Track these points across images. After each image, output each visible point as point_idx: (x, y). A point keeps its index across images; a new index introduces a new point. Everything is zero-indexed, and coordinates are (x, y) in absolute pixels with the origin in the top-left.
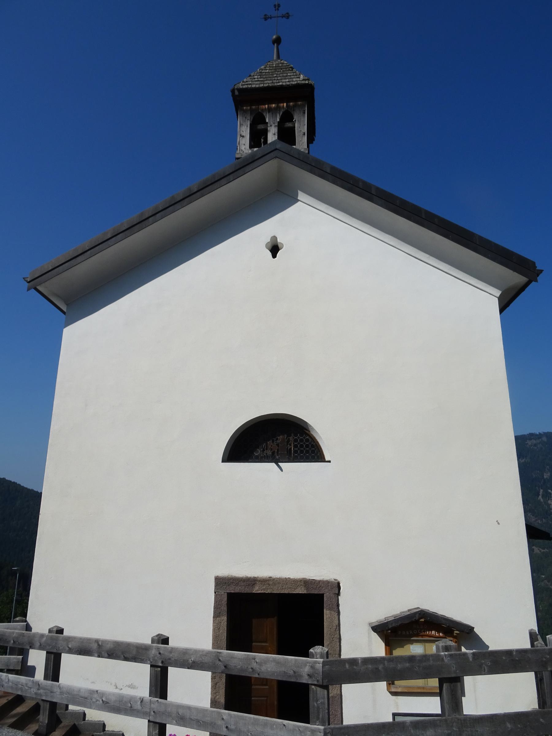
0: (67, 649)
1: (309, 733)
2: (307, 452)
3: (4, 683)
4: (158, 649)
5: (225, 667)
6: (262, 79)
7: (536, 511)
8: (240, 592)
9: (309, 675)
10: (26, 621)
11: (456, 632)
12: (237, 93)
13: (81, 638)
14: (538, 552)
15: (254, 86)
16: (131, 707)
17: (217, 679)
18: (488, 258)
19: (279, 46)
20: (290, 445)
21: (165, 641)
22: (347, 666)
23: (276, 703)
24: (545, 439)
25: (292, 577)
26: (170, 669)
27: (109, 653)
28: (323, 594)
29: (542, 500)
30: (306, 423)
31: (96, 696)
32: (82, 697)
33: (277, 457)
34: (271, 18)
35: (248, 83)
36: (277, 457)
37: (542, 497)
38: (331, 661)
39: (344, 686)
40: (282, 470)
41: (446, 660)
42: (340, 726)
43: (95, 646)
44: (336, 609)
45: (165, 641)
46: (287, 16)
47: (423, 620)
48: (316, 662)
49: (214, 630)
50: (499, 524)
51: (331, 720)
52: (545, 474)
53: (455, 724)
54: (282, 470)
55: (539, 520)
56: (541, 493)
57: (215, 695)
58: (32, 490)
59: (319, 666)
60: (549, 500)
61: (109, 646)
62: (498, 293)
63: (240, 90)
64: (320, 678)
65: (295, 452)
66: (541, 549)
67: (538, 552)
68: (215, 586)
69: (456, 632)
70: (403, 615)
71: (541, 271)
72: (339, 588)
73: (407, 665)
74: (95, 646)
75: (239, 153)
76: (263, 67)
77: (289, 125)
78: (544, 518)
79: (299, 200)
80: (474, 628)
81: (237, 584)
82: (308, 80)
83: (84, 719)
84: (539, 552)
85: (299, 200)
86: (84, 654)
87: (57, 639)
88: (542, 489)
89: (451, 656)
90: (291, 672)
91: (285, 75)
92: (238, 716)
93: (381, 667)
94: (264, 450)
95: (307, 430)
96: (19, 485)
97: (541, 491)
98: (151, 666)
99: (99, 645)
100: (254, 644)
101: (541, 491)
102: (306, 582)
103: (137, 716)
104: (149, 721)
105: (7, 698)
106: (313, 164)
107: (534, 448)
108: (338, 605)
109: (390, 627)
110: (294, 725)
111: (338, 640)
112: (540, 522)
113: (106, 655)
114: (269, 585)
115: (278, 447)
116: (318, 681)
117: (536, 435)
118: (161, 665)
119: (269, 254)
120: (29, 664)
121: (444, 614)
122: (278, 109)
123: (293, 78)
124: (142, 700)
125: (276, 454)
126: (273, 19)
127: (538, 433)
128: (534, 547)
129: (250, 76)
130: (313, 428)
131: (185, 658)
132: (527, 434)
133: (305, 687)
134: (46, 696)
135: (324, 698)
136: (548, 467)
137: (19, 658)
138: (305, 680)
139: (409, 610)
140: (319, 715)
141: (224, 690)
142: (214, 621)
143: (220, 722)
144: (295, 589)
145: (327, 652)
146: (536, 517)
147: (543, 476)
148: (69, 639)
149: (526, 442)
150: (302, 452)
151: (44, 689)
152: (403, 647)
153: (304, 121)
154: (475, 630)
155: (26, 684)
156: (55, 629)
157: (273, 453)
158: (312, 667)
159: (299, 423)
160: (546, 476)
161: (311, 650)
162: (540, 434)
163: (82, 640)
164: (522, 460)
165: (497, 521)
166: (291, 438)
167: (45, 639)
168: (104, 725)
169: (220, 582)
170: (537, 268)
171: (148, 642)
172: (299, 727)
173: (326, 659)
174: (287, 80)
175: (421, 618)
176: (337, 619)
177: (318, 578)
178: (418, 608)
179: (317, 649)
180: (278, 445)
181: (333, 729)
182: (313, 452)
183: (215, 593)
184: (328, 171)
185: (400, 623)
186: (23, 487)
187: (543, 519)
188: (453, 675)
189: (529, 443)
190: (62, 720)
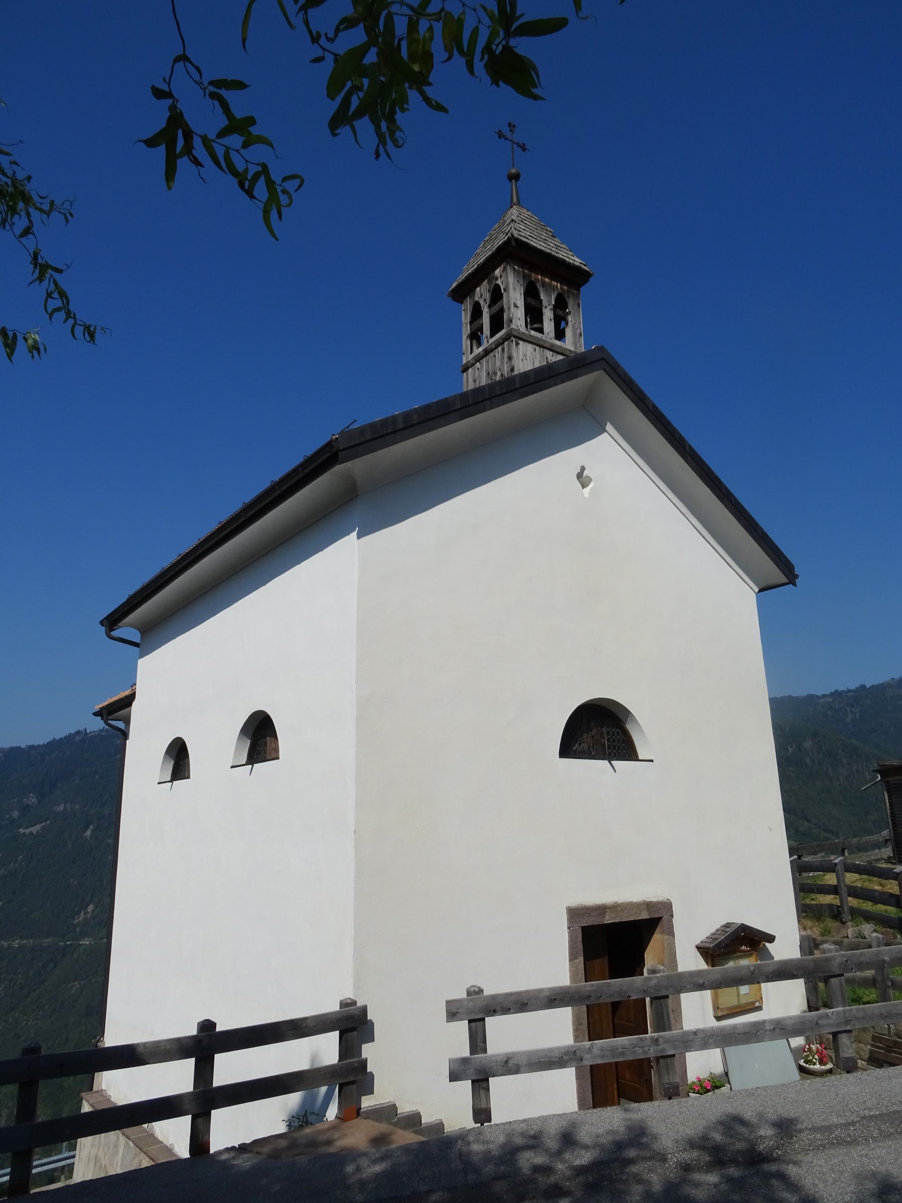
20: (604, 738)
27: (849, 962)
32: (739, 1034)
33: (593, 753)
94: (580, 744)
95: (623, 723)
102: (649, 905)
106: (638, 394)
114: (618, 912)
115: (593, 740)
122: (554, 288)
130: (634, 720)
159: (614, 710)
169: (574, 913)
178: (728, 925)
180: (593, 737)
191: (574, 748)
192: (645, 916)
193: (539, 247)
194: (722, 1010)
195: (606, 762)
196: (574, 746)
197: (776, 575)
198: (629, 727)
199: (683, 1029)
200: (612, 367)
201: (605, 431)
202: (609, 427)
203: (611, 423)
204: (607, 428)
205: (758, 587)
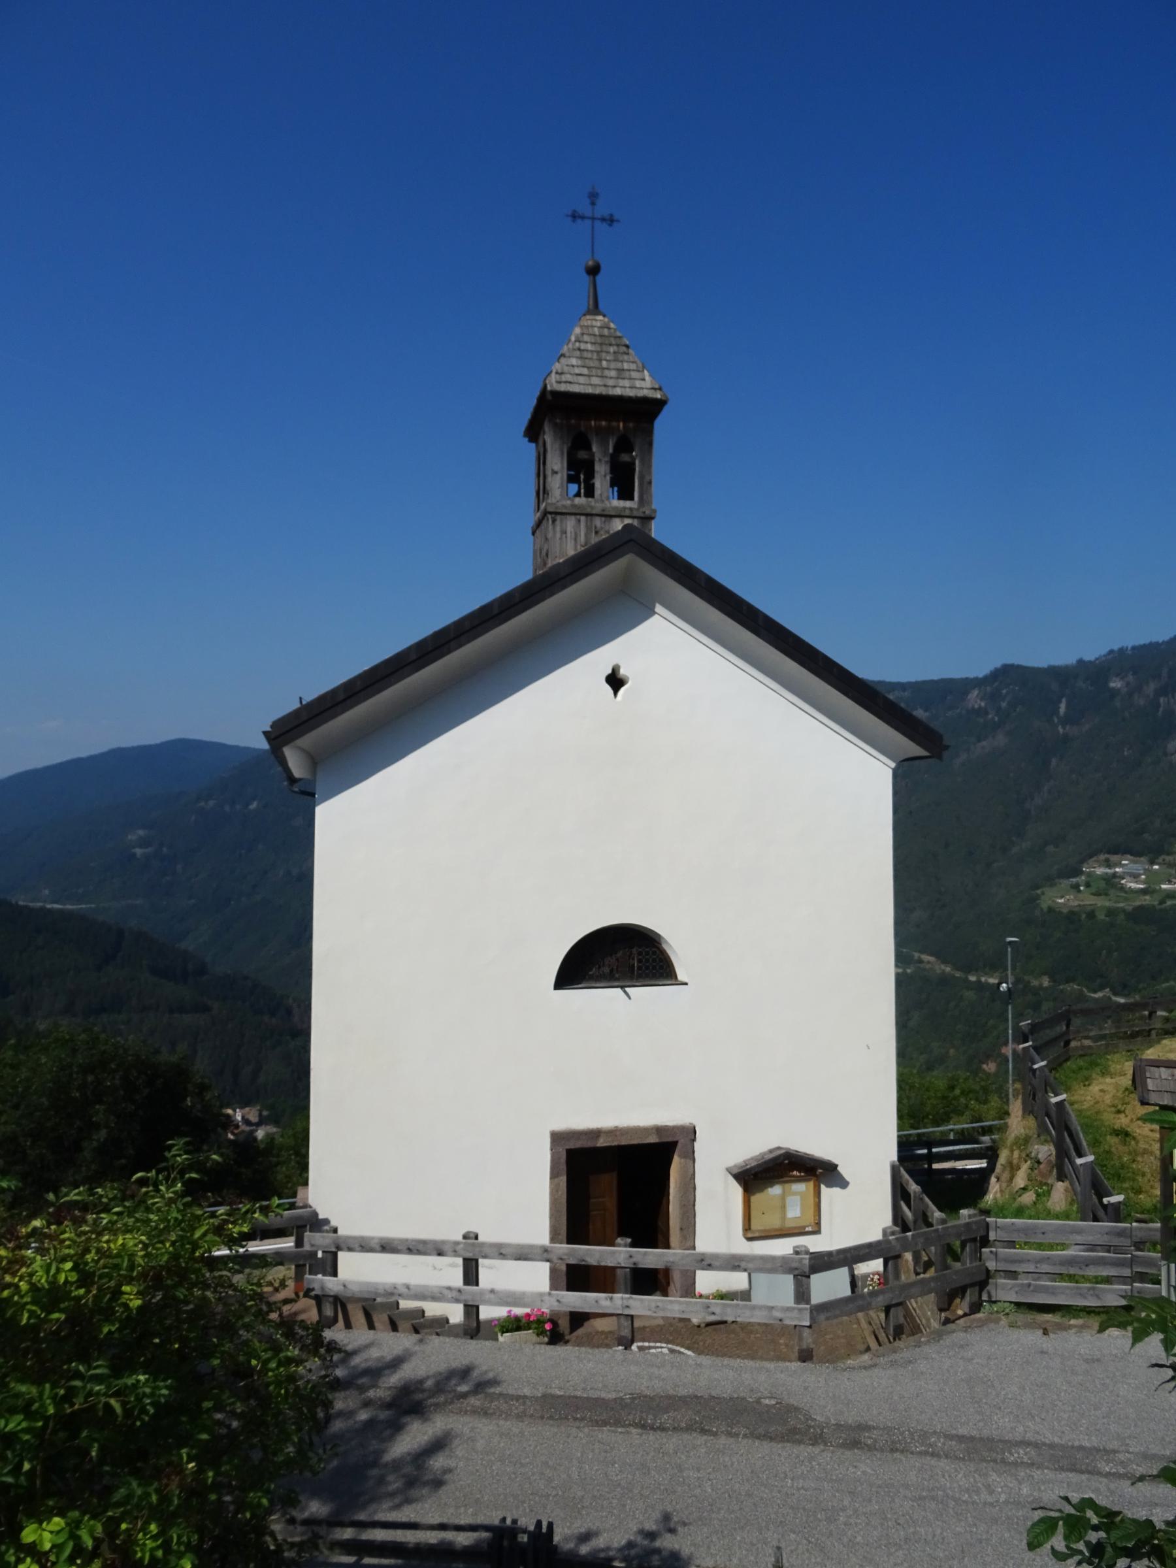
2: (654, 968)
6: (585, 371)
13: (519, 1245)
20: (633, 959)
22: (826, 1258)
30: (659, 935)
33: (617, 976)
36: (617, 976)
40: (630, 998)
46: (610, 221)
47: (787, 1162)
48: (802, 1259)
50: (869, 1048)
54: (630, 998)
62: (893, 765)
65: (639, 968)
72: (695, 1132)
73: (867, 1251)
77: (625, 457)
79: (656, 613)
80: (837, 1166)
82: (660, 389)
83: (398, 1308)
85: (656, 613)
94: (599, 967)
102: (659, 1130)
105: (508, 1309)
108: (694, 1152)
130: (666, 942)
139: (771, 1151)
150: (647, 968)
154: (839, 1168)
157: (612, 971)
166: (634, 951)
168: (423, 1312)
169: (557, 1138)
174: (627, 383)
175: (785, 1160)
178: (779, 1148)
180: (617, 960)
182: (661, 967)
191: (591, 973)
192: (653, 1139)
193: (589, 390)
194: (754, 1232)
195: (619, 990)
196: (591, 970)
198: (665, 946)
199: (694, 1248)
200: (641, 546)
201: (655, 613)
202: (659, 608)
205: (894, 761)
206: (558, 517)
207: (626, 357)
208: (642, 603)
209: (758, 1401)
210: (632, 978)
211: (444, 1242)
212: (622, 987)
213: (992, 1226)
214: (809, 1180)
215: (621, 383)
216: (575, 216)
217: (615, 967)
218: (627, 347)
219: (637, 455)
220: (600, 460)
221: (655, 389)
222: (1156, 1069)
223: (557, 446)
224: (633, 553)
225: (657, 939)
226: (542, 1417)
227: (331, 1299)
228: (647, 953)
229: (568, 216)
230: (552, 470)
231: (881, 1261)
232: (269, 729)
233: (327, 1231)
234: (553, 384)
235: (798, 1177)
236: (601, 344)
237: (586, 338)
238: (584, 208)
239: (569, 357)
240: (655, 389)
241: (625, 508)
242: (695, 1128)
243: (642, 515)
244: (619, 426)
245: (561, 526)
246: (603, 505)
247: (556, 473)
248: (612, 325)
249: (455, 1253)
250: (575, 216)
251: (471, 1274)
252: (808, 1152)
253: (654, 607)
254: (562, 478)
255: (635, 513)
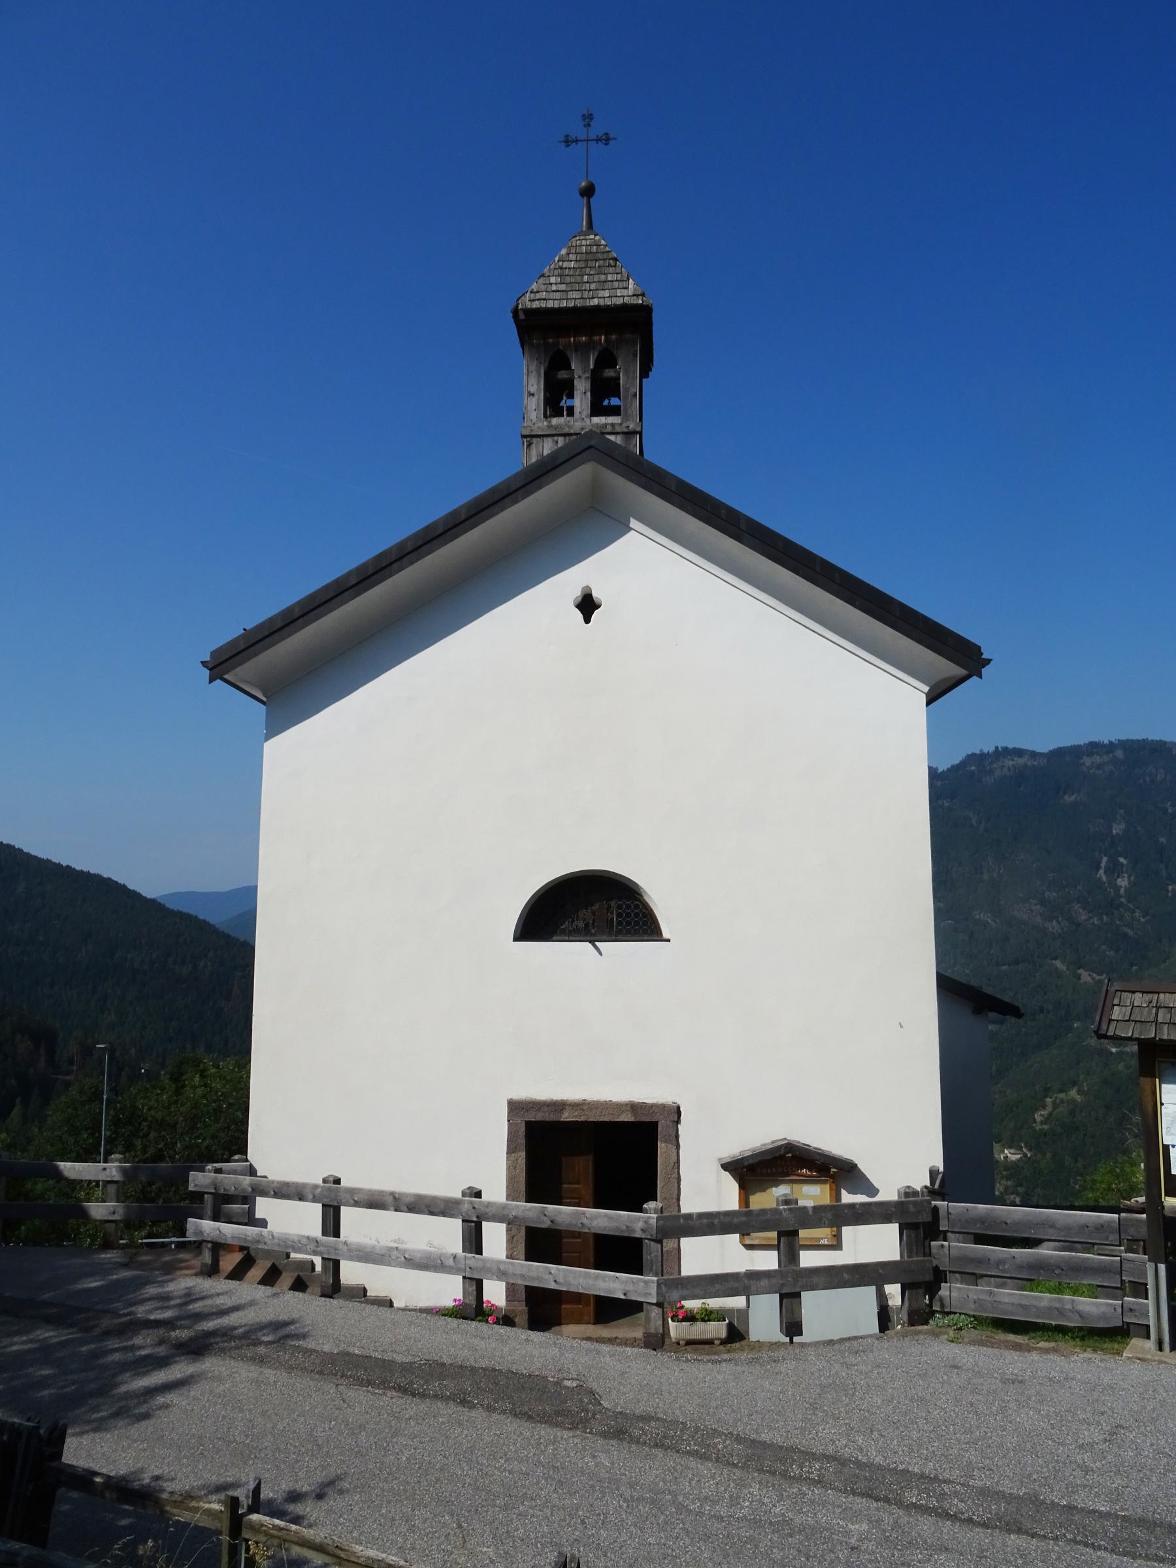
0: (352, 1201)
1: (642, 1284)
2: (637, 923)
3: (266, 1240)
4: (471, 1202)
5: (552, 1222)
6: (563, 287)
7: (1090, 900)
8: (543, 1119)
9: (642, 1230)
10: (247, 1160)
11: (833, 1170)
12: (522, 316)
13: (370, 1191)
14: (1089, 979)
15: (550, 304)
16: (442, 1263)
17: (514, 1232)
18: (912, 638)
19: (592, 200)
20: (612, 913)
21: (478, 1194)
22: (682, 1220)
23: (592, 1259)
24: (1119, 754)
25: (614, 1100)
26: (484, 1223)
28: (657, 1122)
29: (1104, 878)
31: (395, 1253)
33: (593, 931)
34: (577, 141)
35: (538, 296)
36: (593, 931)
37: (1105, 872)
38: (666, 1216)
39: (683, 1240)
40: (601, 954)
41: (784, 1214)
42: (675, 1276)
43: (390, 1199)
44: (674, 1141)
45: (478, 1194)
46: (606, 139)
47: (790, 1155)
48: (649, 1217)
49: (508, 1169)
50: (902, 1027)
51: (665, 1271)
52: (1115, 825)
53: (790, 1275)
54: (601, 954)
55: (1096, 919)
56: (1103, 865)
57: (512, 1251)
58: (48, 861)
59: (653, 1222)
60: (1118, 877)
61: (408, 1200)
62: (926, 689)
63: (529, 312)
64: (654, 1232)
65: (619, 923)
66: (1094, 975)
67: (1089, 979)
68: (508, 1113)
69: (833, 1170)
70: (764, 1148)
71: (988, 661)
72: (679, 1113)
73: (744, 1219)
74: (390, 1199)
75: (528, 426)
76: (564, 252)
77: (609, 373)
78: (1107, 915)
81: (539, 1110)
82: (643, 295)
84: (1091, 981)
86: (375, 1208)
87: (337, 1190)
88: (1105, 856)
89: (790, 1210)
90: (624, 1227)
91: (603, 277)
92: (567, 1270)
93: (716, 1221)
94: (573, 921)
96: (20, 850)
97: (1105, 859)
98: (463, 1221)
99: (395, 1198)
100: (564, 1186)
101: (1105, 859)
102: (634, 1107)
103: (450, 1273)
104: (464, 1278)
106: (650, 476)
107: (1097, 772)
108: (677, 1136)
109: (746, 1163)
110: (627, 1277)
111: (676, 1181)
112: (1096, 922)
113: (406, 1209)
114: (583, 1110)
115: (594, 916)
116: (652, 1235)
117: (1104, 746)
118: (475, 1219)
119: (579, 615)
120: (257, 1216)
121: (819, 1147)
122: (589, 346)
123: (616, 289)
124: (455, 1257)
125: (590, 927)
126: (579, 143)
127: (1106, 742)
128: (1081, 971)
129: (543, 275)
130: (645, 892)
131: (505, 1213)
132: (1085, 744)
133: (639, 1242)
134: (329, 1253)
135: (657, 1251)
136: (1122, 811)
137: (244, 1208)
138: (638, 1234)
139: (773, 1142)
140: (652, 1267)
141: (523, 1245)
142: (507, 1158)
143: (547, 1277)
144: (618, 1116)
145: (662, 1208)
146: (1089, 912)
147: (1110, 829)
148: (352, 1191)
149: (1082, 761)
150: (628, 923)
151: (326, 1246)
152: (764, 1191)
153: (635, 372)
155: (300, 1241)
156: (331, 1179)
157: (587, 925)
158: (646, 1222)
160: (1117, 829)
161: (645, 1206)
162: (1111, 743)
163: (372, 1193)
164: (1070, 796)
165: (900, 1024)
166: (613, 903)
167: (319, 1190)
168: (365, 1290)
169: (515, 1107)
170: (983, 657)
171: (459, 1196)
172: (632, 1279)
173: (660, 1215)
174: (606, 293)
176: (675, 1154)
177: (649, 1101)
178: (785, 1139)
179: (651, 1205)
180: (594, 913)
181: (666, 1280)
182: (645, 923)
183: (509, 1121)
184: (673, 488)
185: (759, 1159)
186: (28, 854)
187: (1104, 916)
188: (791, 1229)
189: (1088, 761)
190: (308, 1283)
191: (562, 927)
196: (563, 923)
197: (949, 669)
198: (646, 898)
202: (633, 523)
203: (635, 518)
204: (631, 525)
206: (535, 440)
207: (611, 270)
208: (598, 510)
209: (558, 1383)
210: (610, 934)
211: (304, 1185)
212: (592, 942)
213: (942, 1213)
214: (824, 1182)
215: (601, 293)
216: (568, 141)
217: (591, 922)
218: (616, 260)
219: (620, 368)
220: (580, 377)
221: (637, 295)
222: (1129, 995)
223: (533, 368)
224: (594, 460)
225: (636, 889)
226: (321, 1373)
227: (210, 1245)
228: (628, 907)
229: (560, 142)
230: (529, 392)
231: (774, 1234)
232: (208, 659)
233: (210, 1171)
234: (527, 303)
235: (809, 1176)
236: (586, 261)
237: (572, 257)
238: (578, 131)
239: (549, 276)
240: (637, 295)
241: (606, 425)
242: (678, 1108)
243: (626, 430)
244: (601, 340)
245: (537, 450)
246: (584, 424)
247: (533, 395)
248: (603, 242)
249: (315, 1200)
250: (568, 141)
251: (332, 1225)
252: (823, 1148)
253: (629, 521)
254: (538, 400)
255: (618, 429)
